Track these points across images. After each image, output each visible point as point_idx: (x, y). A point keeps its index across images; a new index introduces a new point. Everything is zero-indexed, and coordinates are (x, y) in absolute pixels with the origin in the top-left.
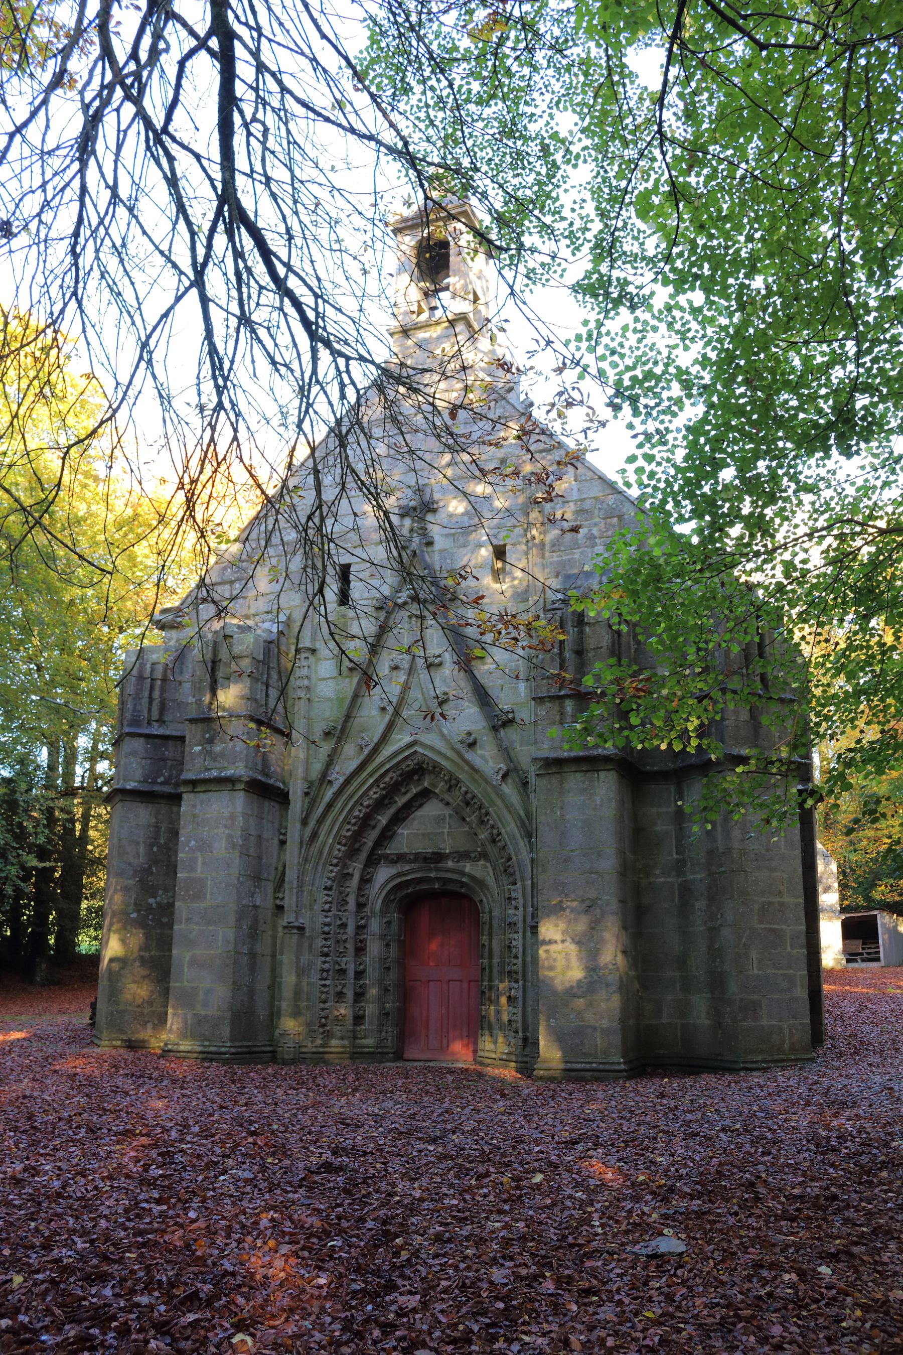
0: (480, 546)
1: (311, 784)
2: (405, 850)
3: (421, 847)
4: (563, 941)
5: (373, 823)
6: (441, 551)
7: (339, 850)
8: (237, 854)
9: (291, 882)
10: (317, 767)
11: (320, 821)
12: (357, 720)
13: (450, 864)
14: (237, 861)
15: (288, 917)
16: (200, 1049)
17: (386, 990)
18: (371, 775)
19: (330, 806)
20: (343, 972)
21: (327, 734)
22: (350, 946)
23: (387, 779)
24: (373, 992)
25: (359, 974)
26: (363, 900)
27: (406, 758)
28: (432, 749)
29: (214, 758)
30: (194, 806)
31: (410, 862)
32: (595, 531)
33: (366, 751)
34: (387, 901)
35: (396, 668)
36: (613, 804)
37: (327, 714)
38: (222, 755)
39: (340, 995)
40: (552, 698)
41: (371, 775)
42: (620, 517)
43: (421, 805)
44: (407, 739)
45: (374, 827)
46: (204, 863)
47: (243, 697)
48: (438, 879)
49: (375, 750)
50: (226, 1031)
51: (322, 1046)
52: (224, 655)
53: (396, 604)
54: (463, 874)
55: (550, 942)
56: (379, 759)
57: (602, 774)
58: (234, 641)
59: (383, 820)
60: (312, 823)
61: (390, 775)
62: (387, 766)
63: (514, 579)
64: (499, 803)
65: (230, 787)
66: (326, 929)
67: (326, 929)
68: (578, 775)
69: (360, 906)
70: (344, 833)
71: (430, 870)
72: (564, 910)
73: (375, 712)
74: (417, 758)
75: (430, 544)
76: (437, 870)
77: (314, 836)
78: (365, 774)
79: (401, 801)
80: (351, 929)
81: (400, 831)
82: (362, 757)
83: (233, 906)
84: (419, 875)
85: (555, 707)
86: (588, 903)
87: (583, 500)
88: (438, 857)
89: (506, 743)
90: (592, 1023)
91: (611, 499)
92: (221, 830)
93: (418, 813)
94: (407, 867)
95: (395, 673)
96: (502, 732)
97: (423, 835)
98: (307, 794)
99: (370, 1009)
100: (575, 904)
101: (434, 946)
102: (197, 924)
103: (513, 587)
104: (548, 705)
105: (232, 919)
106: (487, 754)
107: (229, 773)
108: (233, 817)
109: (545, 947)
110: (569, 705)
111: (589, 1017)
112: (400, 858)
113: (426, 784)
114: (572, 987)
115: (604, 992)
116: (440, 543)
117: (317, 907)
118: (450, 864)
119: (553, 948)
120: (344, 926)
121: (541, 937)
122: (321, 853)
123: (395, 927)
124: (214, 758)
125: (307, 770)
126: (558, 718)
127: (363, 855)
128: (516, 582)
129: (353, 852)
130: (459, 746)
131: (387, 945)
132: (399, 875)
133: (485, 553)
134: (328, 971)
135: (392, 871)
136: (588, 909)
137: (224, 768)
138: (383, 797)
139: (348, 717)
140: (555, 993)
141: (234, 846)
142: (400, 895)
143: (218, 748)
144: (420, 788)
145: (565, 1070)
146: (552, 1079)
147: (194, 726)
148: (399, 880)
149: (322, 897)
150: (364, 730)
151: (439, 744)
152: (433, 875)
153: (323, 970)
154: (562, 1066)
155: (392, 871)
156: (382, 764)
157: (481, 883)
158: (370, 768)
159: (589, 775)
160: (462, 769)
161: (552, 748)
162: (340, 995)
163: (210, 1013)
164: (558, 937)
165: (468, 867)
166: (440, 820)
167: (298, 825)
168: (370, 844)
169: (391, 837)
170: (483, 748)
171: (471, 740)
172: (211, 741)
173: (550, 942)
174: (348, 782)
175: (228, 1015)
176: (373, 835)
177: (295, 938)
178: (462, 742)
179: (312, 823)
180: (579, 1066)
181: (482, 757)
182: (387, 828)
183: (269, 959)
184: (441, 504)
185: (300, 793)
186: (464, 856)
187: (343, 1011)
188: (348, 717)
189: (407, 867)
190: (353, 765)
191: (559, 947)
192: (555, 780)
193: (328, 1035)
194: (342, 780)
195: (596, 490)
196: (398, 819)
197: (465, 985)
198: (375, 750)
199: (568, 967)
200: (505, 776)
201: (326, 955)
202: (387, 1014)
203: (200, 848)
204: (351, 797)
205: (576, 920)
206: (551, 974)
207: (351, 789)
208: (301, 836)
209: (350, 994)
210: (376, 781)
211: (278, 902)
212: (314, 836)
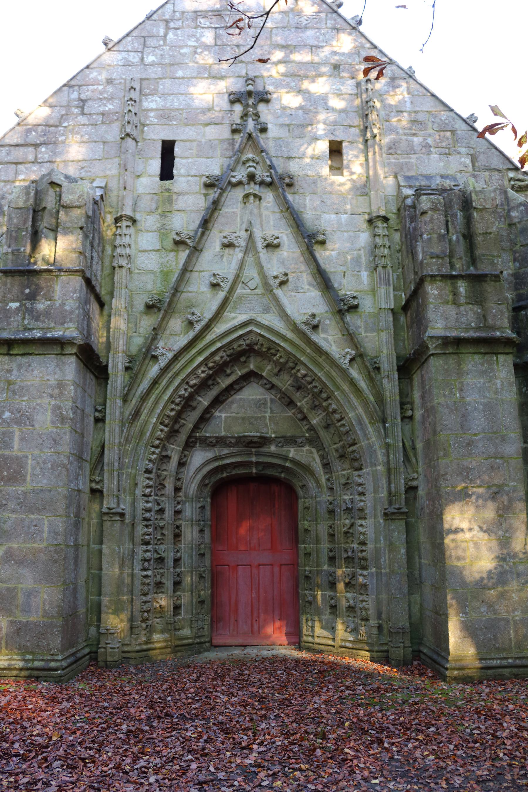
0: (316, 139)
1: (132, 359)
2: (223, 433)
3: (238, 430)
4: (470, 530)
5: (194, 404)
6: (276, 139)
7: (162, 432)
8: (67, 428)
9: (110, 464)
10: (138, 341)
11: (144, 398)
12: (184, 296)
13: (273, 448)
14: (67, 438)
15: (109, 503)
16: (20, 664)
17: (201, 577)
18: (200, 353)
19: (155, 382)
20: (161, 560)
21: (150, 307)
22: (169, 533)
23: (217, 358)
24: (188, 580)
25: (177, 561)
26: (179, 484)
27: (240, 337)
28: (269, 329)
29: (37, 316)
30: (9, 371)
31: (230, 445)
32: (430, 141)
33: (198, 327)
34: (202, 485)
35: (230, 245)
36: (514, 388)
37: (149, 287)
38: (47, 313)
39: (159, 585)
40: (444, 277)
41: (200, 353)
42: (453, 132)
43: (241, 389)
44: (242, 318)
45: (194, 408)
46: (23, 439)
47: (74, 250)
48: (257, 464)
49: (207, 327)
50: (56, 642)
51: (146, 643)
52: (50, 201)
53: (230, 183)
54: (285, 458)
55: (457, 531)
56: (210, 337)
57: (501, 358)
58: (64, 189)
59: (204, 401)
60: (134, 402)
61: (221, 353)
62: (219, 345)
63: (352, 173)
64: (346, 387)
65: (57, 350)
66: (147, 515)
67: (147, 515)
68: (476, 357)
69: (177, 490)
70: (168, 412)
71: (250, 454)
72: (470, 496)
73: (205, 288)
74: (254, 338)
75: (264, 130)
76: (257, 454)
77: (137, 414)
78: (194, 351)
79: (224, 383)
80: (168, 514)
81: (217, 414)
82: (191, 335)
83: (63, 491)
84: (239, 459)
85: (447, 287)
86: (494, 489)
87: (416, 112)
88: (264, 441)
89: (352, 328)
90: (504, 615)
91: (444, 115)
92: (46, 400)
93: (237, 397)
94: (226, 451)
95: (227, 250)
96: (348, 318)
97: (243, 419)
98: (127, 369)
99: (185, 599)
100: (481, 490)
101: (243, 530)
102: (13, 511)
103: (352, 180)
104: (439, 284)
105: (61, 506)
106: (330, 338)
107: (57, 334)
108: (61, 385)
109: (451, 536)
110: (462, 287)
111: (502, 610)
112: (221, 441)
113: (252, 367)
114: (482, 579)
115: (515, 582)
116: (273, 131)
117: (138, 492)
118: (273, 448)
119: (460, 536)
120: (161, 511)
121: (446, 526)
122: (142, 433)
123: (208, 512)
124: (37, 316)
125: (128, 344)
126: (451, 297)
127: (183, 437)
128: (355, 177)
129: (173, 433)
130: (304, 328)
131: (201, 531)
132: (216, 459)
133: (323, 147)
134: (148, 561)
135: (210, 455)
136: (494, 497)
137: (49, 329)
138: (209, 377)
139: (176, 290)
140: (464, 584)
141: (63, 419)
142: (214, 479)
143: (41, 306)
144: (245, 371)
145: (482, 668)
146: (466, 680)
147: (9, 280)
148: (216, 464)
149: (142, 480)
150: (193, 306)
151: (279, 325)
152: (254, 459)
153: (145, 560)
154: (477, 664)
155: (210, 455)
156: (213, 342)
157: (307, 469)
158: (200, 345)
159: (487, 357)
160: (303, 352)
161: (446, 328)
162: (159, 585)
163: (33, 618)
164: (465, 525)
165: (292, 453)
166: (261, 404)
167: (119, 402)
168: (191, 426)
169: (208, 420)
170: (325, 331)
171: (315, 322)
172: (32, 297)
173: (457, 531)
174: (176, 358)
175: (59, 622)
176: (193, 417)
177: (117, 525)
178: (306, 323)
179: (134, 402)
180: (495, 663)
181: (326, 340)
182: (207, 410)
183: (85, 548)
184: (275, 96)
185: (120, 367)
186: (291, 441)
187: (163, 603)
188: (176, 290)
189: (226, 451)
190: (183, 341)
191: (468, 535)
192: (452, 361)
193: (150, 630)
194: (170, 355)
195: (428, 105)
196: (217, 402)
197: (276, 569)
198: (207, 327)
199: (478, 558)
200: (352, 360)
201: (147, 543)
202: (202, 602)
203: (18, 422)
204: (177, 374)
205: (484, 506)
206: (459, 564)
207: (178, 366)
208: (122, 413)
209: (169, 584)
210: (206, 359)
211: (94, 486)
212: (137, 414)
